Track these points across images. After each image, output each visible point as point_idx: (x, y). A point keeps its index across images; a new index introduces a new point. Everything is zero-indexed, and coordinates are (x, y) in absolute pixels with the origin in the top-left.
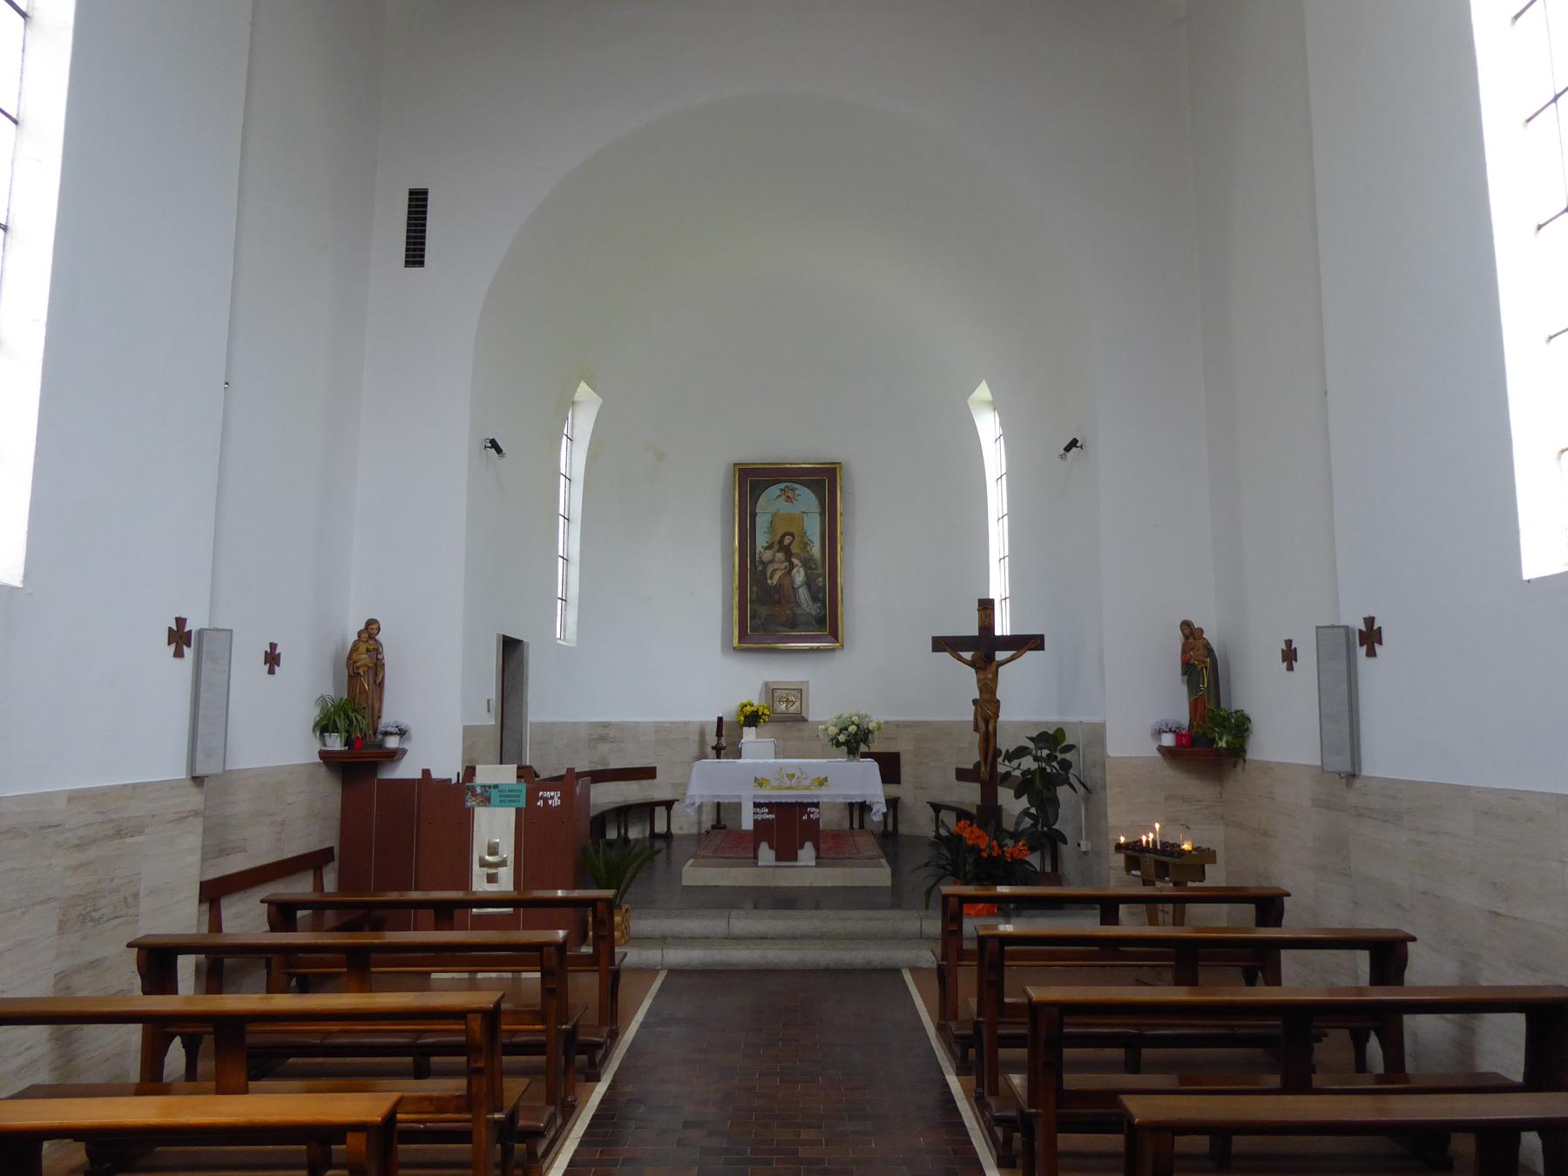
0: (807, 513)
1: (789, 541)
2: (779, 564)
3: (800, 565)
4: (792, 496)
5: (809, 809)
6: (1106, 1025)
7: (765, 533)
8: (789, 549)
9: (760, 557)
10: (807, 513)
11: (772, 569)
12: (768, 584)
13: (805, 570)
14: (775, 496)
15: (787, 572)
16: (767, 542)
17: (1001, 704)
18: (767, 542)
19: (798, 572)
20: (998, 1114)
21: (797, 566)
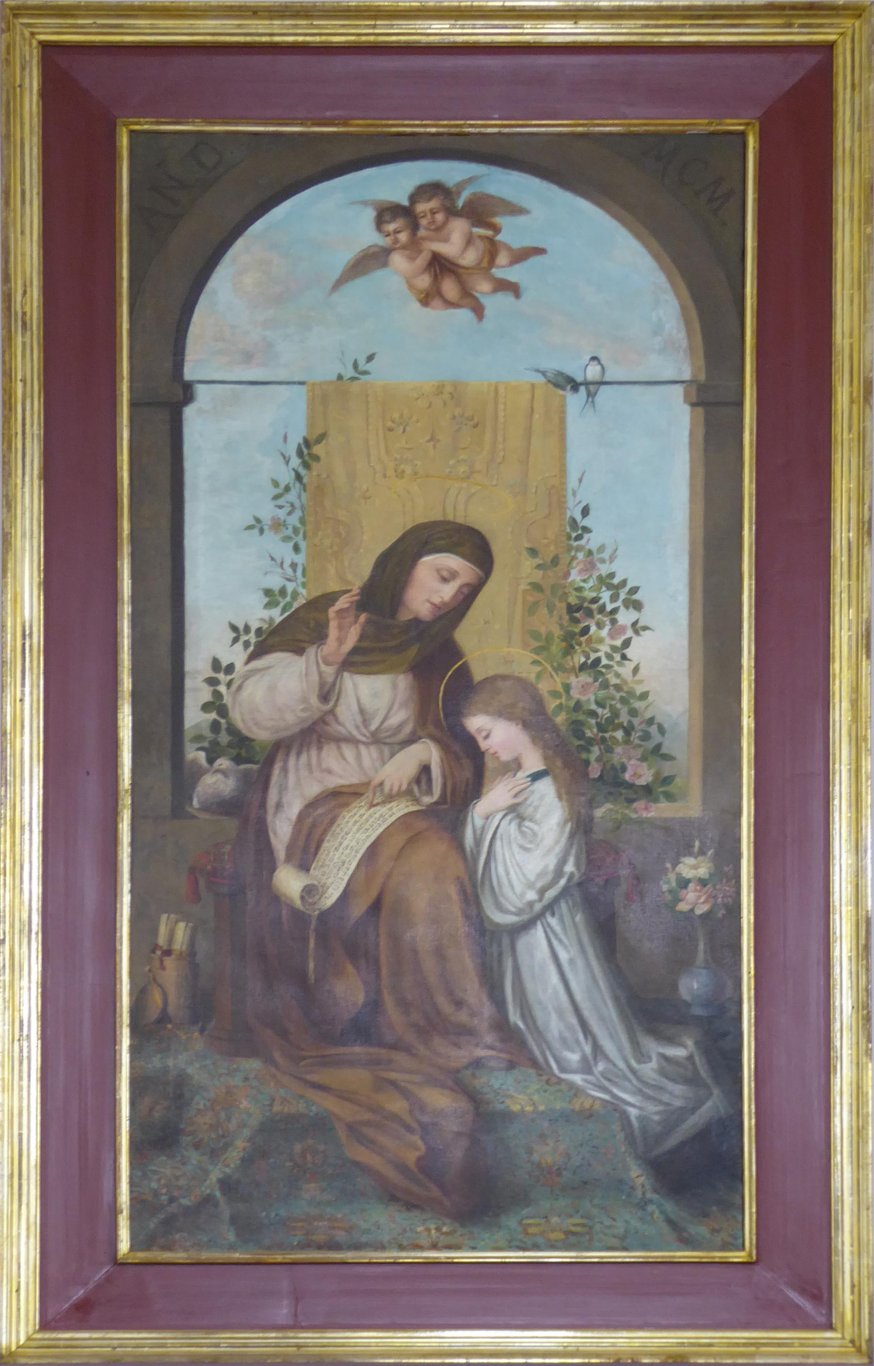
0: (592, 387)
1: (447, 592)
2: (369, 755)
3: (533, 761)
4: (469, 258)
5: (309, 1165)
6: (749, 1059)
7: (257, 525)
8: (453, 652)
9: (216, 705)
10: (592, 387)
11: (313, 790)
12: (276, 899)
13: (567, 792)
14: (344, 257)
15: (430, 812)
16: (271, 597)
17: (588, 517)
18: (271, 597)
19: (515, 811)
20: (124, 141)
21: (516, 765)
